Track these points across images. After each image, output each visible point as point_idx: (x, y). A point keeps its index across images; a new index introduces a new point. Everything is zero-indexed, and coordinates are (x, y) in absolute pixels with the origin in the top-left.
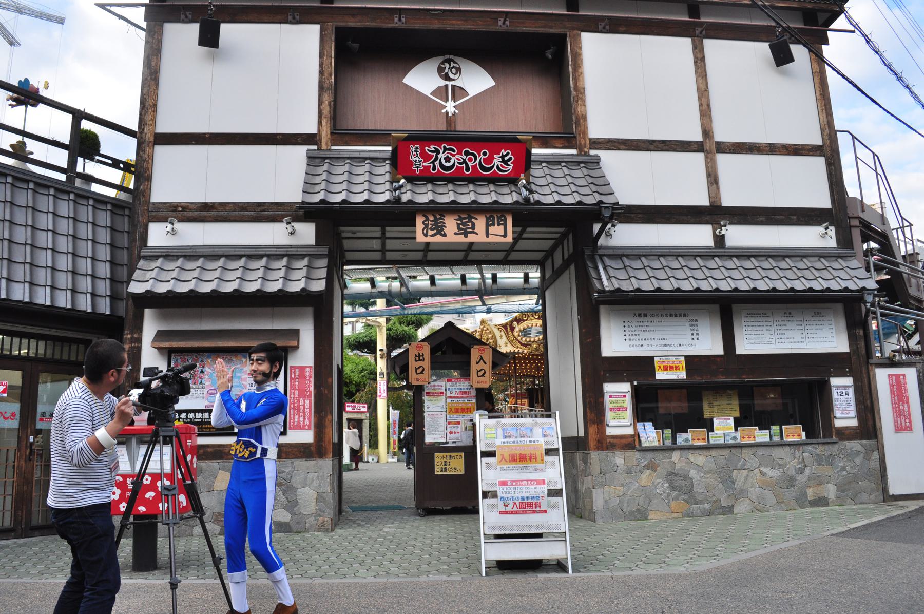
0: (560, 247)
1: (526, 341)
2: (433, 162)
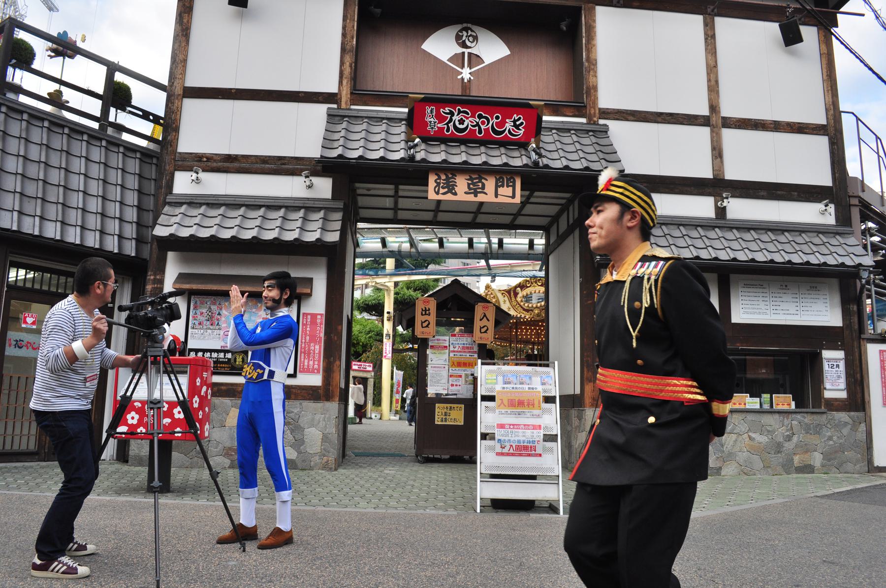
0: (566, 212)
1: (528, 306)
2: (447, 124)
